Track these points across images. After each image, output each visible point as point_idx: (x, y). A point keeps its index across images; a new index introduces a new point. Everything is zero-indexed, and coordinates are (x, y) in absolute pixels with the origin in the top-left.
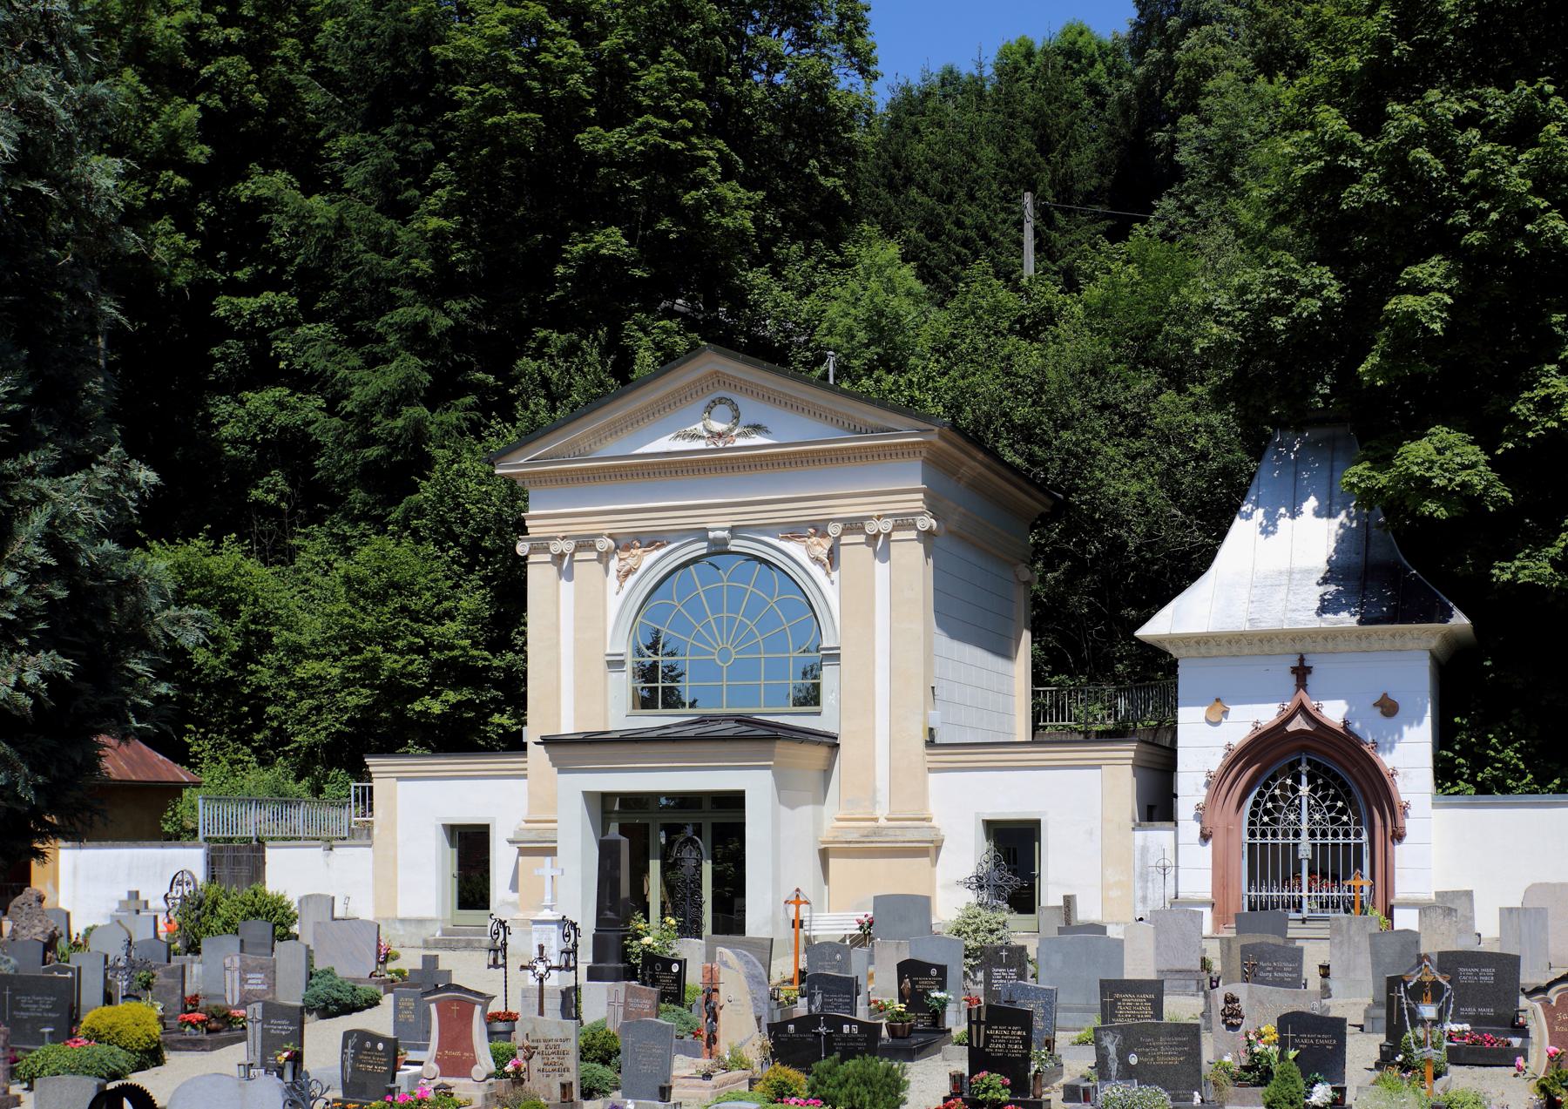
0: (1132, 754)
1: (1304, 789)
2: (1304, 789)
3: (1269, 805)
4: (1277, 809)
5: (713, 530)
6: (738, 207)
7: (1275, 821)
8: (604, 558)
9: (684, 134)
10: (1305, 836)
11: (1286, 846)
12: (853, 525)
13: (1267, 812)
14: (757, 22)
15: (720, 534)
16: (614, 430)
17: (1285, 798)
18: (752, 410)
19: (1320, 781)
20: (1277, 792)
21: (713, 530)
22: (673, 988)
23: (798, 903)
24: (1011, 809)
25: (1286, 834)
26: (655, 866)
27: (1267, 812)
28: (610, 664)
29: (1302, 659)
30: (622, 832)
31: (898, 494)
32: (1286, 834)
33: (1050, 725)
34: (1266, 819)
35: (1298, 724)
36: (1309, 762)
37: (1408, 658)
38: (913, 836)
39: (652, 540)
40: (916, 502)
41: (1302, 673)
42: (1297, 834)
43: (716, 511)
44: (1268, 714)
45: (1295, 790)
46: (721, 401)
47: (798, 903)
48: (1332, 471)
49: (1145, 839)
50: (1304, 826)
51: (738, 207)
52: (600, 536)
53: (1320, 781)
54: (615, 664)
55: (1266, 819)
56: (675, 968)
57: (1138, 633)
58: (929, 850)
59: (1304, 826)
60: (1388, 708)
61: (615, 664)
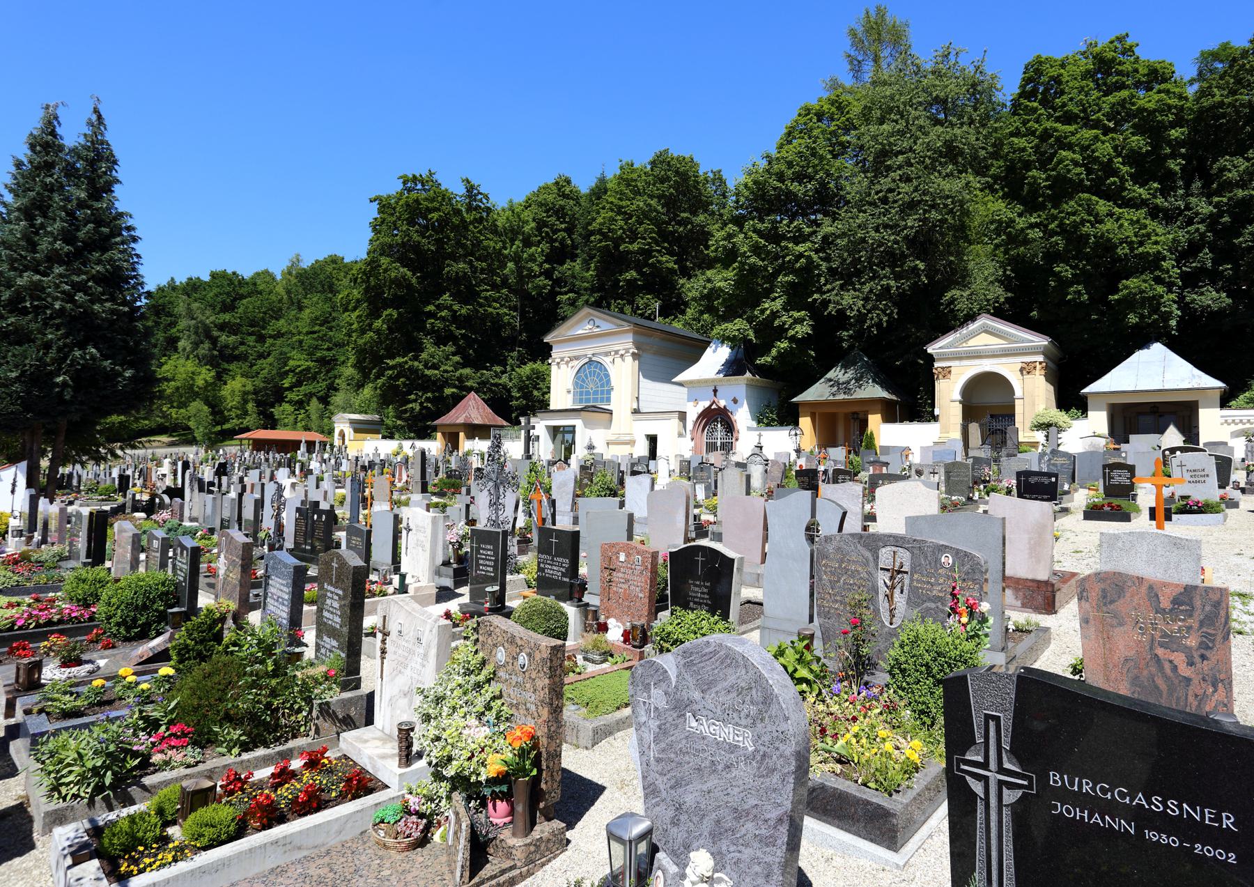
6: (668, 262)
8: (567, 363)
9: (649, 244)
12: (617, 352)
14: (517, 259)
16: (569, 329)
18: (598, 322)
26: (1174, 841)
30: (379, 317)
31: (626, 343)
33: (1215, 597)
35: (714, 407)
37: (740, 385)
38: (627, 438)
39: (577, 358)
40: (631, 345)
41: (715, 391)
43: (588, 349)
44: (707, 404)
51: (668, 262)
58: (632, 443)
60: (735, 401)
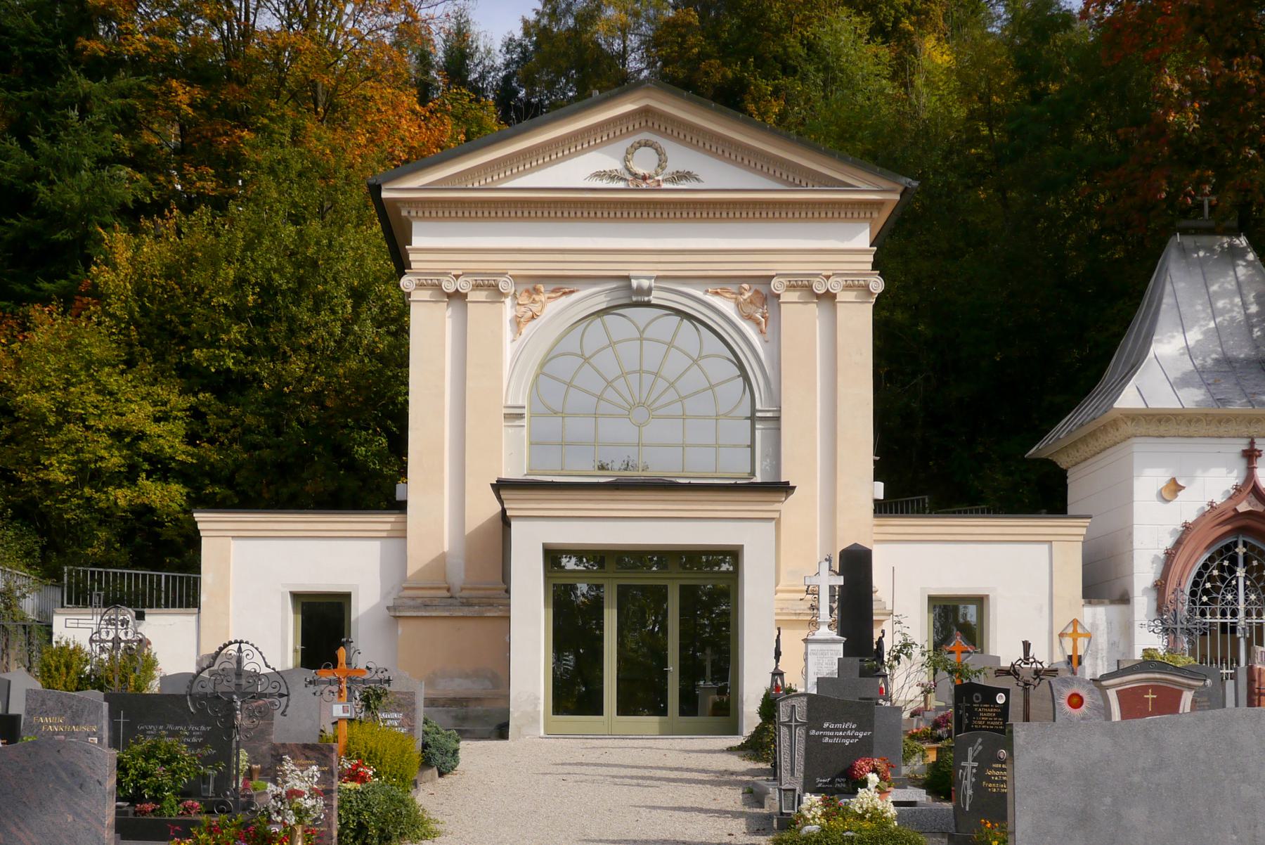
0: (1084, 531)
1: (1241, 572)
2: (1241, 572)
3: (1208, 585)
4: (1216, 589)
5: (637, 278)
7: (1213, 600)
10: (1241, 614)
11: (1224, 625)
13: (1206, 592)
15: (645, 283)
17: (1223, 579)
19: (1255, 563)
20: (1216, 573)
21: (637, 278)
22: (998, 723)
23: (1075, 636)
24: (954, 585)
25: (1224, 614)
27: (1206, 592)
28: (508, 417)
29: (1252, 443)
32: (1224, 614)
34: (1205, 599)
36: (1245, 544)
42: (1234, 613)
45: (1232, 571)
46: (647, 144)
47: (1075, 636)
48: (1204, 274)
49: (1094, 616)
50: (1241, 606)
52: (503, 275)
53: (1255, 563)
54: (514, 416)
55: (1205, 599)
56: (1000, 699)
57: (198, 516)
59: (1241, 606)
61: (514, 416)
